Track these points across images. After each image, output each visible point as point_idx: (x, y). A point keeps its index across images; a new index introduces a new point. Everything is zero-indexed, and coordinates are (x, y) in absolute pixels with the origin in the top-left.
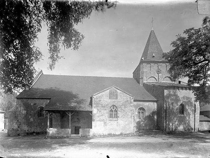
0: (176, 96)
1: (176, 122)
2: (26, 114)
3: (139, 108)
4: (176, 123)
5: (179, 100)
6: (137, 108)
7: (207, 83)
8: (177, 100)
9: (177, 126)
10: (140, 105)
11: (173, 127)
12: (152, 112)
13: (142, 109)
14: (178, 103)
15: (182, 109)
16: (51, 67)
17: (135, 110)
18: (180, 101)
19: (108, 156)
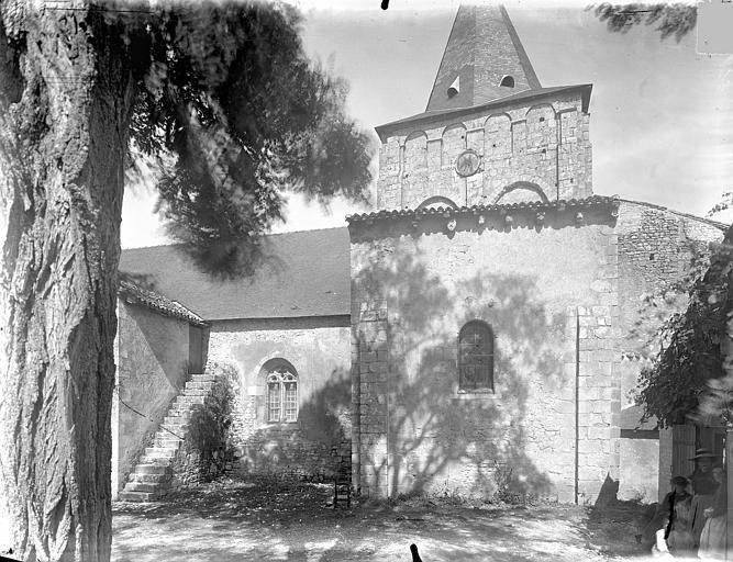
0: (415, 278)
1: (418, 442)
2: (345, 377)
3: (264, 360)
4: (422, 453)
5: (441, 301)
6: (257, 363)
7: (165, 426)
8: (423, 301)
9: (433, 467)
10: (266, 347)
11: (402, 473)
12: (323, 385)
13: (281, 365)
14: (385, 339)
15: (476, 356)
16: (414, 548)
17: (246, 373)
18: (450, 305)
19: (385, 5)
